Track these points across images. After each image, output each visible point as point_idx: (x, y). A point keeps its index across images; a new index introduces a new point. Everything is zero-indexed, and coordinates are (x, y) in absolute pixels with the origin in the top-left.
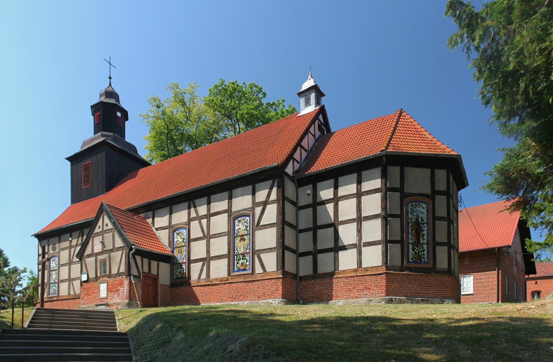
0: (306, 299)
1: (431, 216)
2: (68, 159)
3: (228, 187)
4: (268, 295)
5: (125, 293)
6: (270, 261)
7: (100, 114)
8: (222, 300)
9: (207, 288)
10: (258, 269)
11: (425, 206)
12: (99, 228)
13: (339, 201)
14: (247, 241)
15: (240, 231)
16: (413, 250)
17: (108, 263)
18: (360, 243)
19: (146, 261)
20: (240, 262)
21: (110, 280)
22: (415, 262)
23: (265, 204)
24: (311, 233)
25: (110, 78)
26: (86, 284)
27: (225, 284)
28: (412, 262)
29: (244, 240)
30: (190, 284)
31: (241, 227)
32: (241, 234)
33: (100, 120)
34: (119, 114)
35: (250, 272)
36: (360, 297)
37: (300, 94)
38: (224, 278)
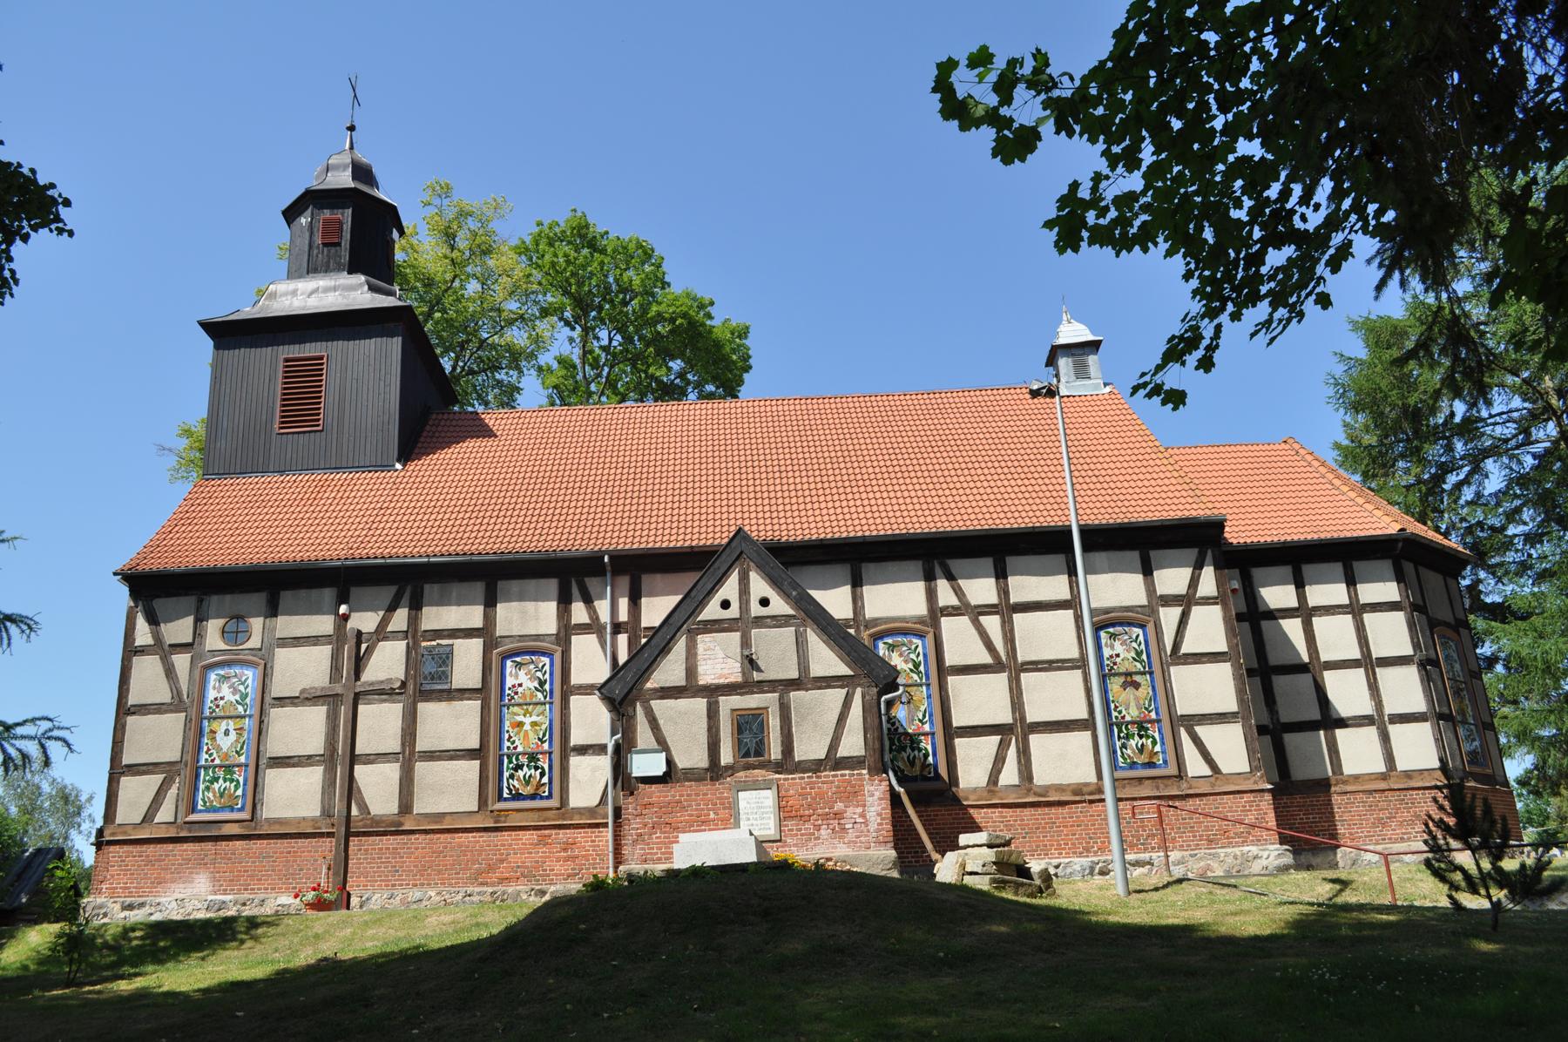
5: (873, 826)
6: (1231, 748)
8: (1087, 850)
9: (1027, 811)
10: (1195, 766)
13: (1311, 616)
14: (1145, 691)
17: (774, 722)
20: (216, 786)
23: (1187, 601)
27: (1091, 802)
29: (1137, 686)
30: (956, 800)
35: (554, 803)
38: (1087, 785)
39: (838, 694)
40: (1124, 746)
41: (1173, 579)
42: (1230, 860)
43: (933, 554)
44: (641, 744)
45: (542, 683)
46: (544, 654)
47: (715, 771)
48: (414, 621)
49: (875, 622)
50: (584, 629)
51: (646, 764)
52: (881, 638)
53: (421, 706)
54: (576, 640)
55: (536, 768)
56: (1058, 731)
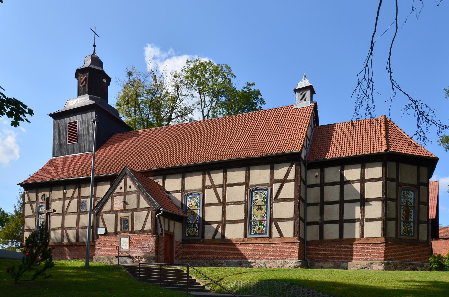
0: (312, 259)
1: (416, 201)
2: (51, 115)
3: (247, 164)
4: (285, 256)
6: (288, 229)
7: (86, 78)
10: (275, 234)
11: (412, 193)
12: (121, 188)
14: (264, 211)
15: (257, 201)
16: (404, 226)
17: (130, 220)
18: (363, 219)
19: (166, 220)
20: (257, 227)
21: (133, 236)
22: (405, 235)
23: (283, 182)
24: (318, 207)
25: (94, 46)
26: (102, 237)
27: (241, 244)
28: (403, 235)
29: (261, 209)
31: (258, 198)
32: (258, 204)
33: (86, 83)
34: (105, 81)
35: (268, 235)
36: (362, 260)
37: (296, 91)
39: (146, 213)
40: (254, 228)
41: (280, 173)
42: (280, 263)
43: (205, 168)
44: (100, 226)
45: (197, 204)
46: (265, 190)
47: (116, 233)
48: (79, 193)
49: (187, 191)
50: (209, 187)
51: (101, 231)
52: (188, 195)
53: (81, 216)
54: (207, 190)
55: (262, 225)
56: (235, 223)
